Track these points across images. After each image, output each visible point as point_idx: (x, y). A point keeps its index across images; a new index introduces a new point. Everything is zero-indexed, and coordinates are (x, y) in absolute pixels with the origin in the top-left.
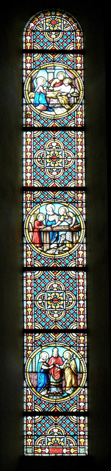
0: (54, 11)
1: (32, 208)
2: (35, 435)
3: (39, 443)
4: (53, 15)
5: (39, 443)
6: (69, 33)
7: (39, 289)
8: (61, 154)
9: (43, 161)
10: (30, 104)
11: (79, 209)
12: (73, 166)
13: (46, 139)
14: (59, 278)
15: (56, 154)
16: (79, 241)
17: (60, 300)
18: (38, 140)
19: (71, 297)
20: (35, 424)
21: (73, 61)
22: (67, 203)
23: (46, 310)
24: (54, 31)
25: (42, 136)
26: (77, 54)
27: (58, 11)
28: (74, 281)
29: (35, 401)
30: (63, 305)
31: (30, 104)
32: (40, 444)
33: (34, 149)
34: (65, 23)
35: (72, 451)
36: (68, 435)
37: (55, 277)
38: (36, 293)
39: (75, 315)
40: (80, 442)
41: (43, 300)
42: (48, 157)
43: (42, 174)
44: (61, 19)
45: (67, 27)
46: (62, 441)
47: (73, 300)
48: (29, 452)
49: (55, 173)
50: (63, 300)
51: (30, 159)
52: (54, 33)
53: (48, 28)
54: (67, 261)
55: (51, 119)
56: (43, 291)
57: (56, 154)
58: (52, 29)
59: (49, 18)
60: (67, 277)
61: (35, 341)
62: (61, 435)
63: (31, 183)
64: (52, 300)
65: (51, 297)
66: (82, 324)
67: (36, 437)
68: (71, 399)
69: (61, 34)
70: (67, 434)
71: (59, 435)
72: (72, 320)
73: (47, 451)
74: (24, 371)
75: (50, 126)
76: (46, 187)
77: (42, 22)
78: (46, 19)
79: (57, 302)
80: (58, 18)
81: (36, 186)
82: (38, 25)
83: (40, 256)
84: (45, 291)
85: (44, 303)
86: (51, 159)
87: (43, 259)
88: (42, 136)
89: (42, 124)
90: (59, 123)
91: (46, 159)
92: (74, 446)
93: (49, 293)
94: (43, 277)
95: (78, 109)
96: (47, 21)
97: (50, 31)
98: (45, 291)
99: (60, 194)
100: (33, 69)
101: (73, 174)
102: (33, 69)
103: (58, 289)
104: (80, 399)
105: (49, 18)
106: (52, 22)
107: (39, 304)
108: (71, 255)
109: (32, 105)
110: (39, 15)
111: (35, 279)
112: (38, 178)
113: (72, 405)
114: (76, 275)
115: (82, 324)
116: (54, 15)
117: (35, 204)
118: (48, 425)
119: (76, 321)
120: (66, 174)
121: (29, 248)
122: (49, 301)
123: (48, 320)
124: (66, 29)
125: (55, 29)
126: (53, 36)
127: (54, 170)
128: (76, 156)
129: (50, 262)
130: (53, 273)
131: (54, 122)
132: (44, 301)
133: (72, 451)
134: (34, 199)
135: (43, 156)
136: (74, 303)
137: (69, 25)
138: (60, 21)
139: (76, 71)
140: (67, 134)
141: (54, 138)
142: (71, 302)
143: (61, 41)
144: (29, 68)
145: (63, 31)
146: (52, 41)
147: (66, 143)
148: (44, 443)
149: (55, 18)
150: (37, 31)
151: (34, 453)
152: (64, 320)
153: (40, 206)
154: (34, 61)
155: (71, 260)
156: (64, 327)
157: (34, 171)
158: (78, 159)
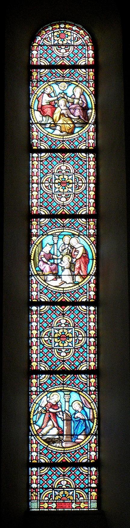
0: (63, 23)
1: (38, 87)
2: (40, 488)
3: (46, 497)
4: (62, 28)
5: (46, 497)
6: (80, 47)
7: (46, 171)
8: (71, 332)
9: (50, 340)
10: (36, 123)
11: (92, 396)
12: (85, 346)
13: (54, 477)
14: (68, 313)
15: (66, 495)
16: (91, 273)
17: (68, 336)
18: (45, 477)
19: (81, 334)
20: (41, 161)
21: (86, 384)
22: (77, 81)
23: (53, 348)
24: (63, 45)
25: (50, 473)
26: (90, 374)
27: (67, 23)
28: (85, 477)
29: (40, 450)
30: (71, 342)
31: (36, 123)
32: (46, 498)
33: (40, 326)
34: (75, 36)
35: (82, 505)
36: (78, 488)
37: (63, 381)
38: (42, 175)
39: (85, 354)
40: (91, 495)
41: (49, 337)
42: (56, 336)
43: (50, 200)
44: (71, 32)
45: (77, 41)
46: (71, 494)
47: (83, 183)
48: (34, 506)
49: (64, 354)
50: (73, 183)
51: (36, 183)
52: (63, 47)
53: (56, 42)
54: (77, 295)
55: (59, 141)
56: (50, 327)
57: (66, 495)
58: (61, 43)
59: (58, 32)
60: (77, 312)
61: (40, 384)
62: (69, 488)
63: (37, 210)
64: (60, 183)
65: (59, 179)
66: (92, 364)
67: (42, 491)
68: (81, 288)
69: (71, 48)
70: (76, 486)
71: (67, 487)
72: (81, 204)
73: (54, 505)
74: (29, 486)
75: (59, 301)
76: (54, 462)
77: (50, 36)
78: (54, 33)
79: (65, 185)
80: (67, 31)
81: (42, 64)
82: (45, 39)
83: (47, 289)
84: (52, 327)
85: (51, 186)
86: (60, 183)
87: (50, 453)
88: (50, 473)
89: (49, 298)
90: (69, 210)
91: (54, 337)
92: (84, 500)
93: (57, 491)
94: (50, 159)
95: (91, 440)
96: (55, 34)
97: (59, 45)
98: (52, 327)
99: (70, 309)
100: (40, 235)
101: (85, 200)
102: (40, 235)
103: (66, 325)
104: (91, 447)
105: (58, 32)
106: (61, 36)
107: (45, 341)
108: (82, 448)
109: (38, 125)
110: (47, 27)
111: (41, 314)
112: (45, 56)
113: (82, 294)
114: (86, 310)
115: (92, 364)
116: (63, 28)
117: (41, 83)
118: (54, 477)
119: (86, 361)
120: (76, 51)
121: (34, 441)
122: (57, 183)
123: (54, 204)
124: (76, 43)
125: (65, 42)
126: (63, 51)
127: (63, 350)
128: (88, 180)
129: (58, 364)
130: (61, 377)
131: (64, 364)
132: (51, 184)
133: (82, 505)
134: (41, 77)
135: (51, 497)
136: (84, 186)
137: (80, 38)
138: (69, 34)
139: (89, 237)
140: (79, 471)
141: (63, 315)
142: (81, 185)
143: (72, 204)
144: (35, 182)
145: (74, 46)
146: (61, 55)
147: (77, 167)
148: (51, 497)
149: (64, 31)
150: (44, 45)
151: (40, 508)
152: (72, 359)
153: (47, 85)
154: (40, 384)
155: (82, 294)
156: (72, 211)
157: (40, 352)
158: (90, 337)
